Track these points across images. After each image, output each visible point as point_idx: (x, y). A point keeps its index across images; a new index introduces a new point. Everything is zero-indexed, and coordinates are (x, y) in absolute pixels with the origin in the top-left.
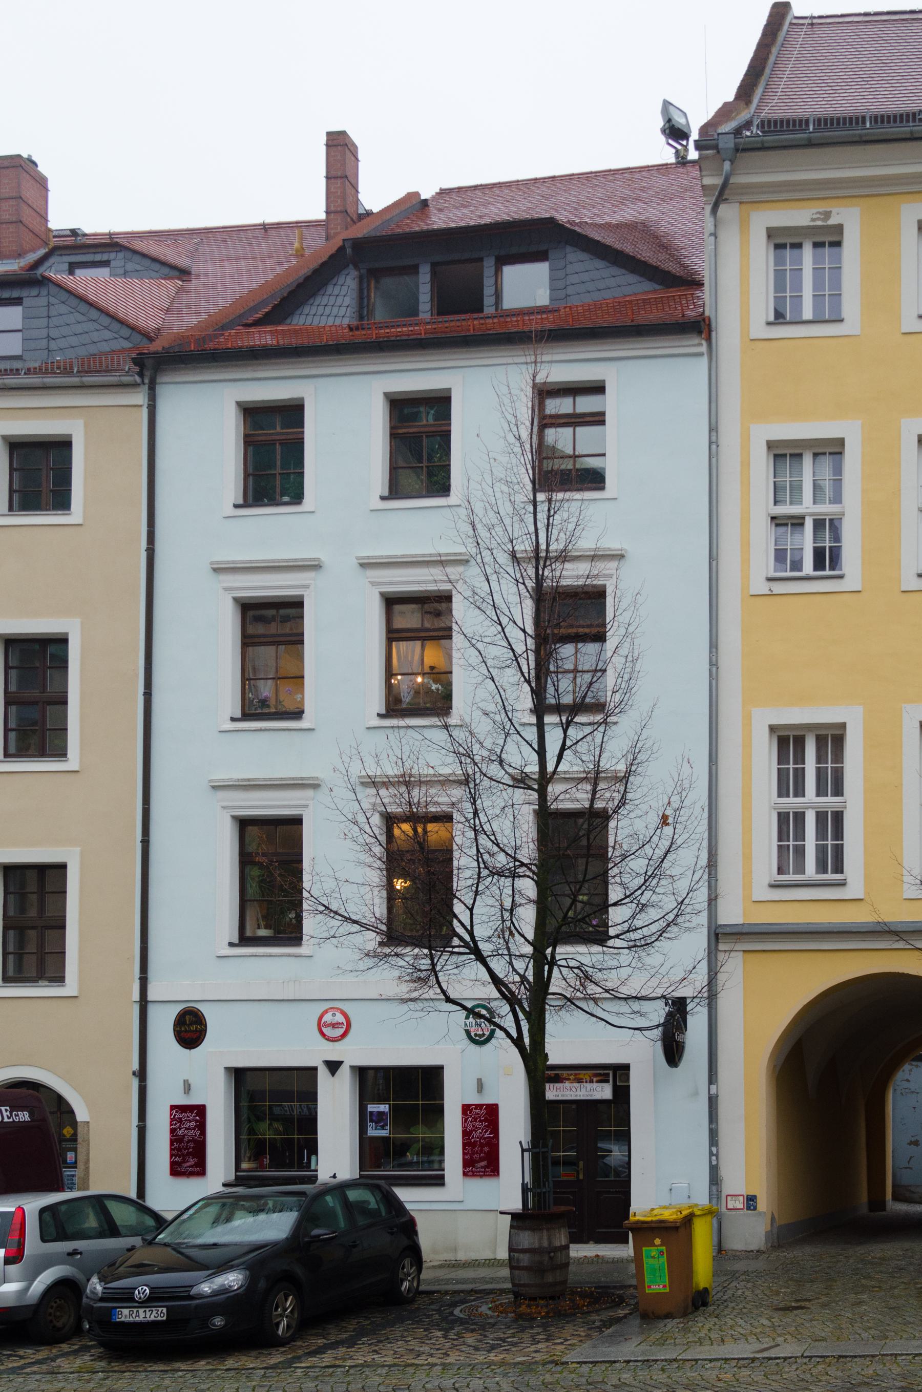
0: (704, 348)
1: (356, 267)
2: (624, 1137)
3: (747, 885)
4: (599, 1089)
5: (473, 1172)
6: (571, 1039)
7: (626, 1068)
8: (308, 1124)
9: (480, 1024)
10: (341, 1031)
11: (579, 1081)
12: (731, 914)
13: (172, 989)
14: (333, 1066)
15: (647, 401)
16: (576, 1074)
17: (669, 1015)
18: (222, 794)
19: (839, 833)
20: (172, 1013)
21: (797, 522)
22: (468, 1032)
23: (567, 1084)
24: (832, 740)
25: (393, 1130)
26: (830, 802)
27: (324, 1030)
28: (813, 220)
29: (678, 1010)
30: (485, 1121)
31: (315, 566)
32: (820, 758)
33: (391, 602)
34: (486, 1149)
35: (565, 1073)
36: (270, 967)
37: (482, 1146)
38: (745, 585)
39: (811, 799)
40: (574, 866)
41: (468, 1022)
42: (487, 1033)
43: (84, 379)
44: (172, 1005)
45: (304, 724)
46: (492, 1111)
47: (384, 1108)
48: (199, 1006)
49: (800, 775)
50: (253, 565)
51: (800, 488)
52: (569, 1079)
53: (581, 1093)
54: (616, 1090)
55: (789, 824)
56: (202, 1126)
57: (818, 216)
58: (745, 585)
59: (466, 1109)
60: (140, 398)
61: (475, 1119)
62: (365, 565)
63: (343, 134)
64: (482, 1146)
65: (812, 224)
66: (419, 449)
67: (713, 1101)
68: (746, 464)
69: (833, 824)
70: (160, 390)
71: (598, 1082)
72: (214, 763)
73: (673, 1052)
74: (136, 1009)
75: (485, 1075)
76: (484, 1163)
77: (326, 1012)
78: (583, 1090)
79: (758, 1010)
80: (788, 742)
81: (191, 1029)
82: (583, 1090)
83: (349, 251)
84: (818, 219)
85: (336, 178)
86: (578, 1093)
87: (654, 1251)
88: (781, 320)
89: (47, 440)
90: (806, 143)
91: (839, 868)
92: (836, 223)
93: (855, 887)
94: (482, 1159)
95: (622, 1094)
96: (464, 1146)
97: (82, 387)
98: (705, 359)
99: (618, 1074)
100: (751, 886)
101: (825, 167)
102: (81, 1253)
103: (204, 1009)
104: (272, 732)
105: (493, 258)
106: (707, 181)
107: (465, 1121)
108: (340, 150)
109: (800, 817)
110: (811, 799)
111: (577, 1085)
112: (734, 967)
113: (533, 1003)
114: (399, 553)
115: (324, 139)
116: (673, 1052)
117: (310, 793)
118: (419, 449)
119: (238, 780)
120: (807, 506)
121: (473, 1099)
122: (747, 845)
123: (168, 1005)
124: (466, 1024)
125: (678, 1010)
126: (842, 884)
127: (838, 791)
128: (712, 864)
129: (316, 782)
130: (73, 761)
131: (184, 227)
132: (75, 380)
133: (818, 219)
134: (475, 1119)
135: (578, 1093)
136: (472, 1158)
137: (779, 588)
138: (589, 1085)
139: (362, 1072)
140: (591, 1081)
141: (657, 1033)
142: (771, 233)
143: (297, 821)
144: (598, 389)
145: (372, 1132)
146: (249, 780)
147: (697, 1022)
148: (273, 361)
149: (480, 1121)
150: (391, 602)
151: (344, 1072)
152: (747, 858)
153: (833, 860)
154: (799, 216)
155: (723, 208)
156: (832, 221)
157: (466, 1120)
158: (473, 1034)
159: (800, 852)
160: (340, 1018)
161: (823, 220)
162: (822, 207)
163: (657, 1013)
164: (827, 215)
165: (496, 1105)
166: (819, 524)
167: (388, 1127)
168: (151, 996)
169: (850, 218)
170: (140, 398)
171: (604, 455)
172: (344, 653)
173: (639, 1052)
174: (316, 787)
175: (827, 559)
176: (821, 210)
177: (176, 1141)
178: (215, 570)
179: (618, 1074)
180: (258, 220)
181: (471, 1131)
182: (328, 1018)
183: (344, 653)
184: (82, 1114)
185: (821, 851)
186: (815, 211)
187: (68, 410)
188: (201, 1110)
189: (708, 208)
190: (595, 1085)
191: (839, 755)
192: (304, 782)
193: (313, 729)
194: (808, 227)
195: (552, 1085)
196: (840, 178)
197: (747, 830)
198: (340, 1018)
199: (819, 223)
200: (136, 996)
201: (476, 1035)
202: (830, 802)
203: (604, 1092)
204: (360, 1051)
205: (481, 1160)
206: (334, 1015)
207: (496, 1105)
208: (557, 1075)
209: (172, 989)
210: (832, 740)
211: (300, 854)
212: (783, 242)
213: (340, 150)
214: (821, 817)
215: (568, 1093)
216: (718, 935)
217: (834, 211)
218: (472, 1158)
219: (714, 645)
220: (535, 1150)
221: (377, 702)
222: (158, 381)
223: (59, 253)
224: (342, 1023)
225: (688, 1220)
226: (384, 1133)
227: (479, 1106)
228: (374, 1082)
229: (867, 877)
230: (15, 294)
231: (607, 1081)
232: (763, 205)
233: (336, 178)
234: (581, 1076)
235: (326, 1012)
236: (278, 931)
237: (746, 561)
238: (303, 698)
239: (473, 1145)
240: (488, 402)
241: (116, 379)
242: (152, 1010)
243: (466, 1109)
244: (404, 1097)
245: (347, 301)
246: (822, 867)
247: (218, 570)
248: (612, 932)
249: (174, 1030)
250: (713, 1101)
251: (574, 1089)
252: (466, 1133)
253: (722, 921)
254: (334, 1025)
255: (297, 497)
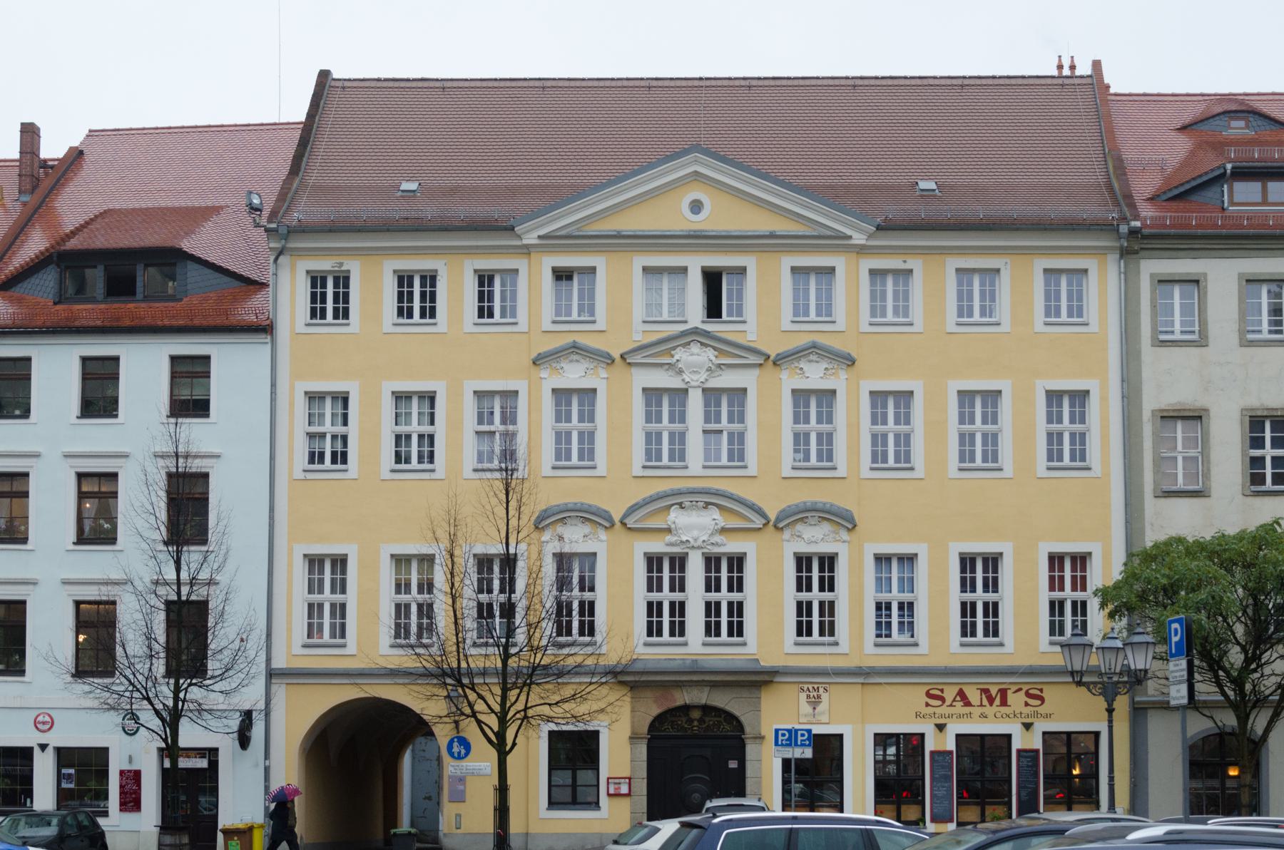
0: (269, 340)
1: (58, 266)
2: (214, 791)
3: (289, 646)
6: (190, 735)
7: (216, 750)
8: (28, 780)
9: (132, 724)
12: (279, 663)
14: (43, 747)
15: (234, 367)
17: (243, 721)
19: (343, 616)
21: (323, 436)
24: (340, 563)
25: (77, 784)
26: (338, 597)
29: (247, 716)
31: (36, 455)
32: (333, 572)
33: (81, 476)
38: (291, 473)
39: (327, 596)
40: (188, 625)
45: (28, 547)
46: (137, 774)
47: (72, 771)
49: (321, 581)
51: (324, 415)
54: (210, 762)
55: (314, 610)
58: (291, 473)
59: (122, 772)
62: (67, 456)
63: (32, 125)
66: (99, 396)
67: (267, 770)
68: (292, 404)
69: (340, 610)
73: (244, 741)
75: (136, 752)
79: (294, 719)
80: (315, 562)
87: (234, 843)
91: (343, 636)
93: (352, 648)
94: (131, 801)
95: (214, 765)
96: (121, 794)
98: (269, 346)
99: (211, 754)
100: (291, 648)
106: (272, 245)
107: (121, 780)
108: (30, 133)
109: (321, 606)
110: (327, 596)
112: (280, 691)
113: (172, 719)
115: (19, 128)
116: (244, 741)
117: (31, 587)
118: (99, 396)
120: (327, 427)
121: (126, 767)
122: (289, 623)
125: (247, 716)
126: (344, 646)
127: (343, 591)
128: (269, 635)
137: (310, 476)
139: (59, 751)
141: (236, 735)
143: (24, 602)
145: (64, 785)
147: (257, 732)
150: (81, 476)
151: (50, 750)
152: (289, 630)
153: (340, 631)
155: (281, 259)
159: (321, 626)
160: (47, 719)
163: (235, 723)
164: (341, 264)
166: (334, 437)
169: (914, 263)
173: (226, 745)
174: (35, 584)
175: (340, 457)
177: (123, 793)
179: (211, 754)
182: (40, 718)
185: (333, 626)
189: (272, 258)
191: (344, 572)
197: (289, 614)
198: (47, 719)
202: (338, 597)
203: (203, 763)
204: (59, 738)
210: (340, 563)
211: (25, 622)
213: (30, 133)
214: (333, 606)
216: (272, 674)
219: (272, 518)
221: (72, 535)
225: (251, 829)
226: (72, 786)
228: (65, 756)
229: (358, 644)
236: (8, 666)
237: (291, 459)
238: (27, 529)
240: (144, 367)
243: (122, 772)
244: (84, 767)
245: (52, 284)
246: (333, 636)
248: (210, 673)
250: (267, 770)
252: (121, 787)
253: (275, 665)
254: (44, 723)
255: (26, 414)
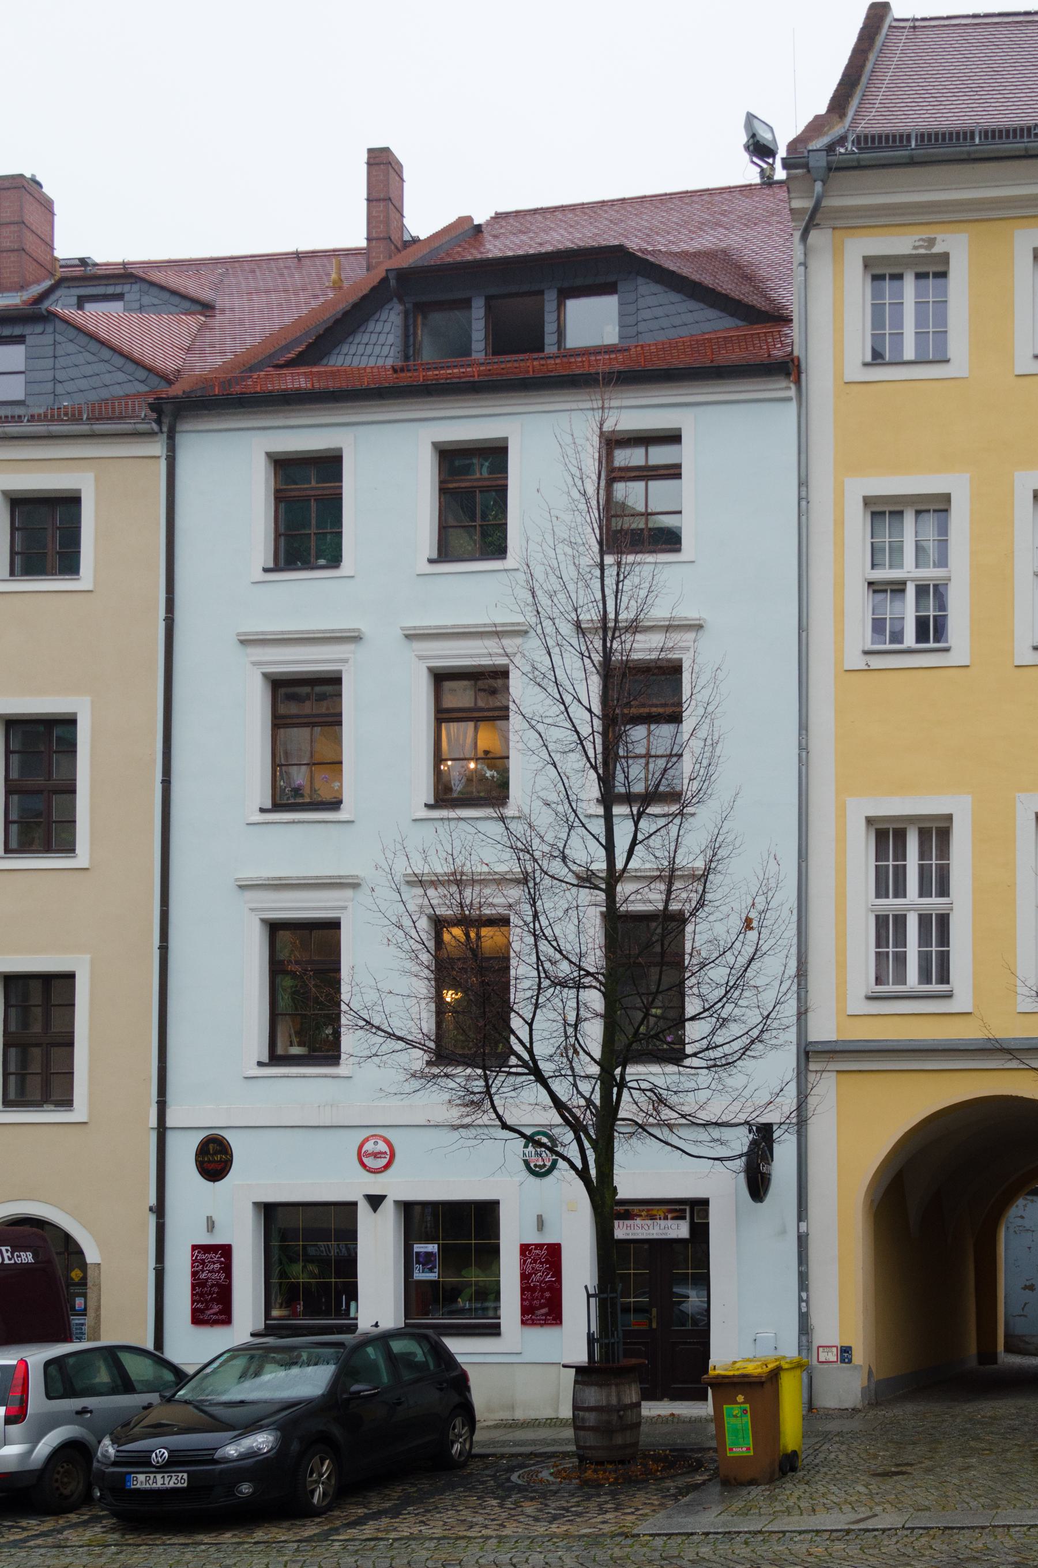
0: (792, 392)
1: (401, 301)
2: (703, 1281)
3: (841, 996)
4: (674, 1227)
5: (533, 1320)
6: (643, 1170)
7: (705, 1203)
8: (347, 1267)
9: (541, 1153)
10: (383, 1162)
11: (652, 1217)
12: (823, 1029)
13: (193, 1114)
14: (375, 1201)
15: (728, 452)
16: (648, 1210)
17: (754, 1143)
18: (249, 895)
19: (944, 939)
20: (194, 1141)
21: (897, 588)
22: (527, 1163)
23: (639, 1221)
24: (937, 833)
25: (443, 1273)
26: (934, 903)
27: (365, 1160)
28: (915, 248)
29: (763, 1138)
30: (546, 1262)
31: (354, 638)
32: (923, 854)
33: (440, 678)
34: (547, 1295)
35: (636, 1209)
36: (304, 1089)
37: (543, 1290)
38: (839, 659)
39: (913, 900)
40: (646, 975)
41: (526, 1151)
42: (548, 1164)
43: (95, 427)
44: (194, 1133)
45: (342, 815)
46: (554, 1252)
47: (432, 1248)
48: (224, 1134)
49: (901, 873)
50: (285, 636)
51: (901, 550)
52: (640, 1216)
53: (654, 1232)
54: (694, 1228)
55: (888, 929)
56: (227, 1268)
57: (921, 243)
58: (839, 659)
59: (525, 1249)
60: (157, 448)
61: (535, 1261)
62: (411, 637)
63: (386, 150)
64: (543, 1290)
65: (914, 252)
66: (472, 506)
67: (802, 1241)
68: (839, 523)
69: (937, 928)
70: (180, 439)
71: (673, 1218)
72: (240, 859)
73: (758, 1185)
74: (153, 1137)
75: (546, 1211)
76: (545, 1310)
77: (367, 1140)
78: (657, 1228)
79: (853, 1138)
80: (887, 835)
81: (215, 1159)
82: (657, 1228)
83: (393, 282)
84: (921, 247)
85: (378, 200)
86: (651, 1231)
87: (736, 1410)
88: (879, 361)
89: (53, 495)
90: (908, 161)
91: (944, 978)
92: (941, 251)
93: (963, 999)
94: (543, 1305)
95: (700, 1232)
96: (523, 1290)
97: (92, 436)
98: (794, 405)
99: (695, 1210)
100: (846, 998)
101: (929, 188)
102: (91, 1412)
103: (230, 1137)
104: (306, 825)
105: (556, 291)
106: (796, 204)
107: (523, 1263)
108: (383, 169)
109: (900, 921)
110: (913, 900)
111: (649, 1222)
112: (826, 1089)
113: (601, 1130)
114: (449, 623)
115: (365, 157)
116: (758, 1185)
117: (349, 893)
118: (472, 506)
119: (268, 879)
120: (908, 570)
121: (533, 1238)
122: (841, 951)
123: (189, 1132)
124: (524, 1154)
125: (763, 1138)
126: (948, 996)
127: (944, 890)
128: (802, 974)
129: (355, 881)
130: (83, 857)
131: (207, 255)
132: (84, 428)
133: (921, 247)
134: (535, 1261)
135: (651, 1231)
136: (531, 1304)
137: (876, 662)
138: (663, 1223)
139: (407, 1208)
140: (666, 1218)
141: (740, 1164)
142: (868, 262)
143: (334, 925)
144: (673, 438)
145: (419, 1275)
146: (280, 879)
147: (784, 1151)
148: (307, 407)
149: (541, 1263)
150: (440, 678)
151: (388, 1208)
152: (841, 966)
153: (938, 968)
154: (899, 244)
155: (813, 234)
156: (937, 249)
157: (525, 1262)
158: (532, 1165)
159: (901, 959)
160: (382, 1147)
161: (926, 248)
162: (925, 233)
163: (740, 1141)
164: (932, 242)
165: (559, 1245)
166: (922, 591)
167: (436, 1270)
168: (170, 1122)
169: (956, 245)
170: (157, 448)
171: (680, 512)
172: (387, 735)
173: (720, 1185)
174: (355, 886)
175: (931, 630)
176: (924, 237)
177: (198, 1285)
178: (242, 642)
179: (695, 1210)
180: (291, 248)
181: (530, 1275)
182: (369, 1147)
183: (387, 735)
184: (92, 1255)
185: (924, 959)
186: (917, 237)
187: (77, 462)
188: (226, 1251)
189: (797, 235)
190: (670, 1222)
191: (944, 851)
192: (342, 881)
193: (353, 822)
194: (910, 256)
195: (621, 1222)
196: (946, 201)
197: (841, 935)
198: (382, 1147)
199: (922, 251)
200: (153, 1122)
201: (536, 1166)
202: (934, 903)
203: (680, 1230)
204: (405, 1184)
205: (542, 1306)
206: (376, 1143)
207: (559, 1245)
208: (627, 1211)
209: (193, 1114)
210: (937, 833)
211: (338, 962)
212: (882, 272)
213: (383, 169)
214: (924, 920)
215: (640, 1231)
216: (809, 1053)
217: (939, 237)
218: (531, 1304)
219: (803, 727)
220: (602, 1296)
221: (425, 791)
222: (178, 429)
223: (66, 285)
224: (385, 1153)
225: (775, 1374)
226: (432, 1276)
227: (539, 1246)
228: (421, 1219)
229: (976, 988)
230: (17, 331)
231: (684, 1218)
232: (859, 230)
233: (378, 200)
234: (654, 1212)
235: (367, 1140)
236: (313, 1049)
237: (839, 632)
238: (341, 787)
239: (532, 1290)
240: (550, 453)
241: (130, 426)
242: (171, 1138)
243: (525, 1249)
244: (454, 1236)
245: (391, 339)
246: (925, 976)
247: (245, 642)
248: (689, 1050)
249: (196, 1161)
250: (802, 1241)
251: (646, 1227)
252: (524, 1277)
253: (813, 1037)
254: (376, 1155)
255: (335, 560)
